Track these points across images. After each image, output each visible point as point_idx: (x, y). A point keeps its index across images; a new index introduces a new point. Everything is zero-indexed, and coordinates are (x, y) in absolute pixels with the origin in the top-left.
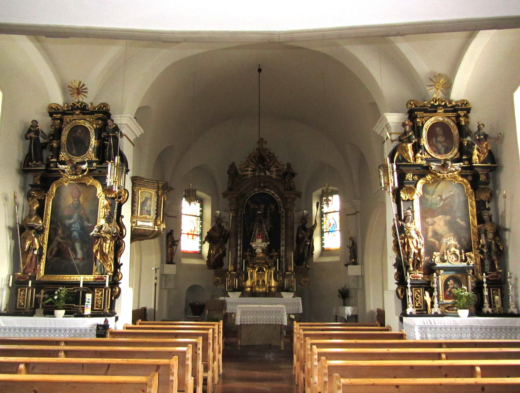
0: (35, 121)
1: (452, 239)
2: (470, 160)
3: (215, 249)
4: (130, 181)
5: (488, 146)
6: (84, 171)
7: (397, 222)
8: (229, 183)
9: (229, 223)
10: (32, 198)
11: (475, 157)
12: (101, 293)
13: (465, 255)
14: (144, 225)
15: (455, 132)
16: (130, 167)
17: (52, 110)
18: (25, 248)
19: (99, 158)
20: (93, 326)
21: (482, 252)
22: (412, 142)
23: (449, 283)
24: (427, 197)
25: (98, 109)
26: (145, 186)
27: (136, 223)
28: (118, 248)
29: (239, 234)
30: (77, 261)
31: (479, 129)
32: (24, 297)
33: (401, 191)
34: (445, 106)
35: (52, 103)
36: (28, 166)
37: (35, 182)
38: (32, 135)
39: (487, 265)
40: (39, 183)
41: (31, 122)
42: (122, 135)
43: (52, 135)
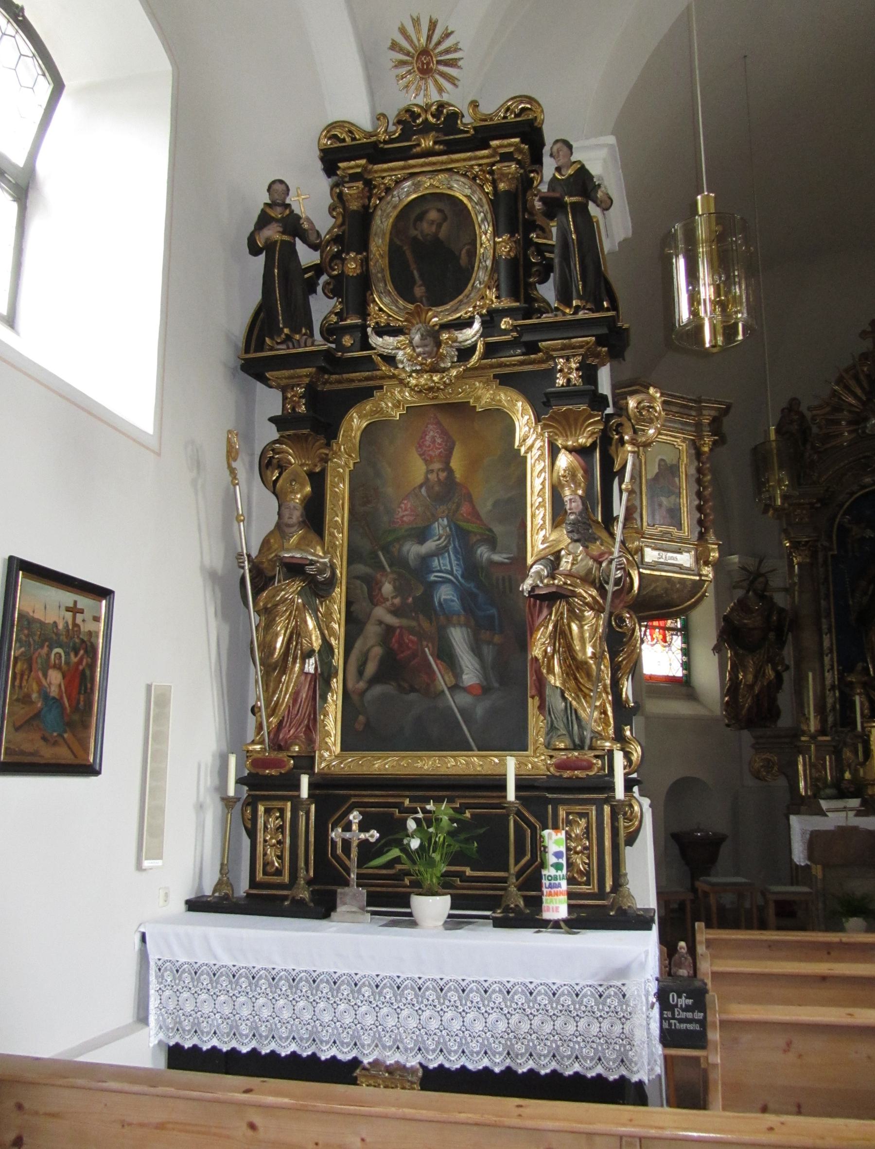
0: (281, 182)
3: (750, 664)
6: (465, 353)
12: (583, 822)
18: (275, 648)
20: (607, 979)
30: (464, 699)
32: (280, 837)
36: (260, 347)
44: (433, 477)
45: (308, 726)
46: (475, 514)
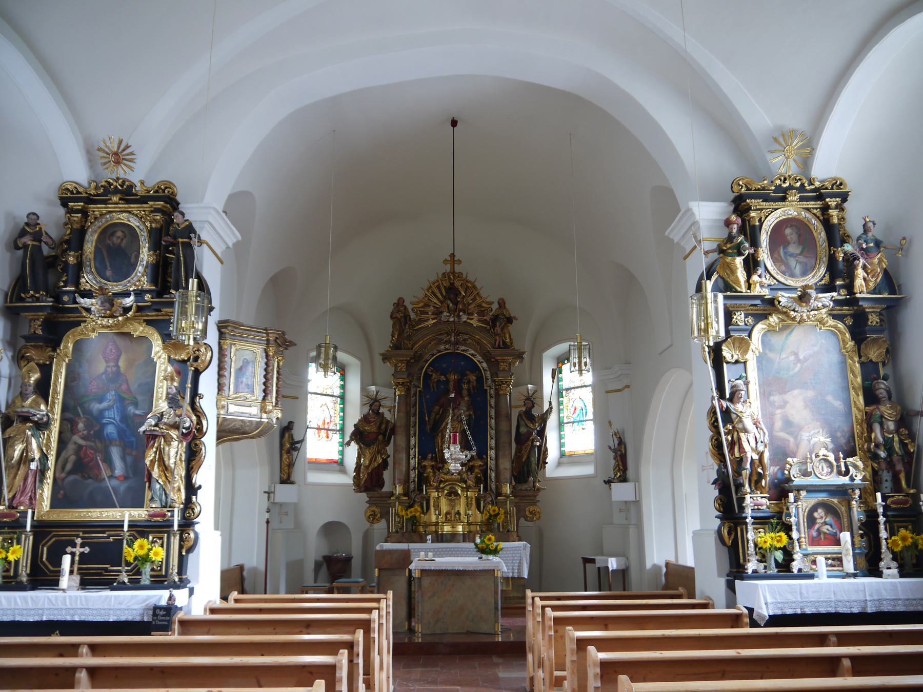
0: (34, 214)
1: (821, 432)
2: (850, 287)
3: (368, 456)
4: (216, 328)
5: (883, 261)
6: (127, 310)
7: (719, 401)
8: (393, 336)
9: (395, 407)
10: (26, 362)
11: (859, 282)
13: (845, 463)
14: (242, 413)
15: (821, 235)
16: (215, 302)
17: (67, 194)
19: (156, 285)
21: (875, 457)
22: (743, 255)
23: (816, 515)
24: (771, 355)
25: (154, 192)
26: (242, 338)
27: (226, 408)
28: (193, 457)
29: (412, 429)
31: (866, 230)
33: (724, 345)
34: (802, 188)
35: (65, 180)
37: (32, 330)
38: (27, 240)
39: (886, 481)
40: (39, 332)
41: (26, 215)
42: (201, 242)
43: (67, 242)
44: (109, 369)
45: (31, 497)
46: (129, 390)
